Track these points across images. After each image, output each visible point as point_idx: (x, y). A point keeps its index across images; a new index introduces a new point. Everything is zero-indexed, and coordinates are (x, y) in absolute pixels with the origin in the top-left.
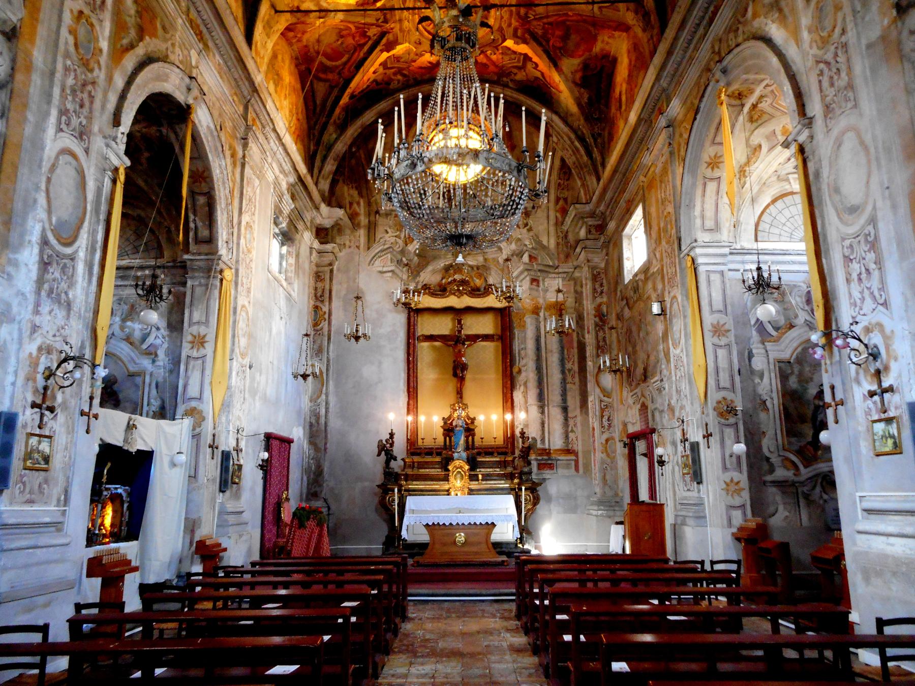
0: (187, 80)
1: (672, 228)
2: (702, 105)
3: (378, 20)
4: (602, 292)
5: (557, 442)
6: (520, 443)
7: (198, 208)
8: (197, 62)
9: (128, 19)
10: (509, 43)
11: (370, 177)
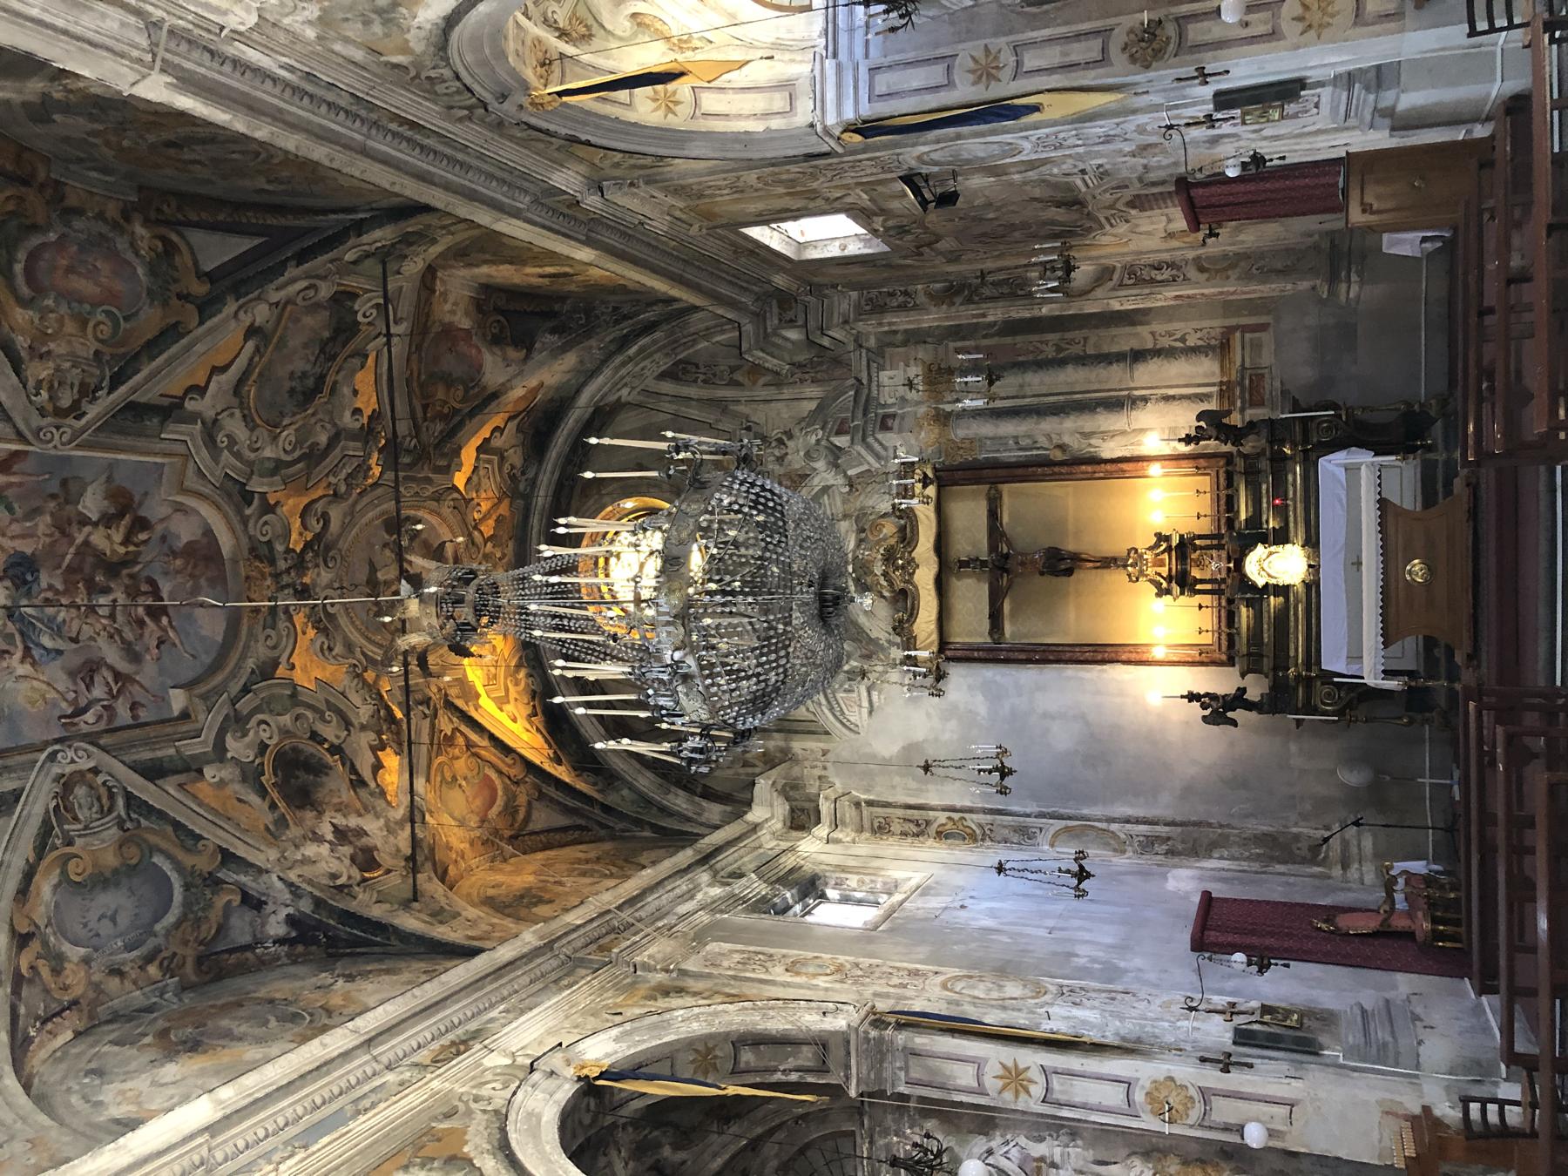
0: (536, 1076)
1: (788, 171)
2: (563, 131)
3: (426, 716)
4: (906, 293)
5: (1205, 371)
6: (1211, 445)
7: (762, 1064)
8: (505, 1053)
10: (460, 480)
11: (704, 770)
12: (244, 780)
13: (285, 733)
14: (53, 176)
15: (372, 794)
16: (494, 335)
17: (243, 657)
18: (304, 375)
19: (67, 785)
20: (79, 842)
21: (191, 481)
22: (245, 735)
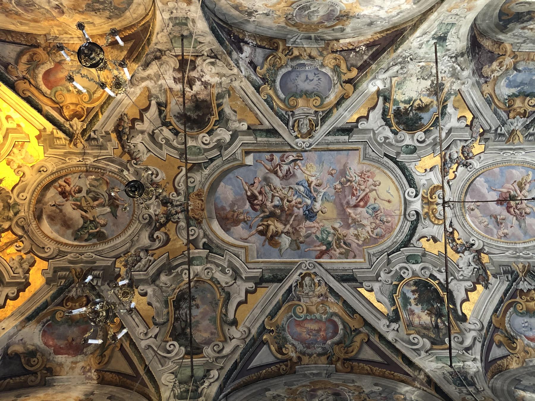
14: (334, 366)
17: (210, 175)
19: (309, 134)
20: (312, 111)
21: (242, 252)
22: (219, 140)
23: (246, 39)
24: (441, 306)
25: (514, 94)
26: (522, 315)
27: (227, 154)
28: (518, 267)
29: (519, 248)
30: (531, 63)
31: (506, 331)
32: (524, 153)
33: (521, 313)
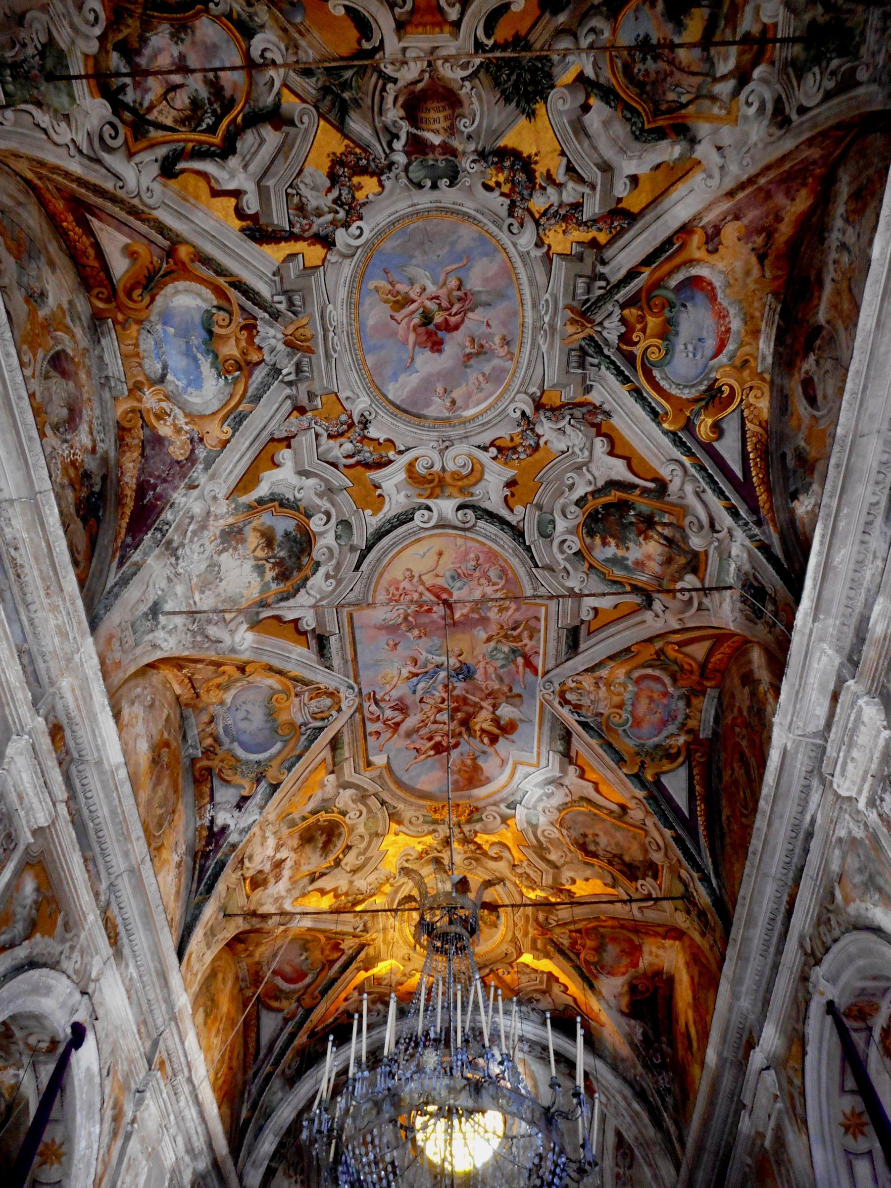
3: (355, 929)
9: (19, 909)
10: (527, 958)
12: (324, 800)
13: (352, 829)
15: (304, 887)
16: (637, 986)
17: (405, 801)
18: (597, 844)
20: (296, 700)
22: (353, 801)
23: (207, 824)
24: (634, 509)
25: (213, 365)
26: (669, 352)
27: (371, 787)
28: (577, 335)
29: (534, 321)
30: (142, 347)
31: (697, 400)
32: (330, 307)
33: (666, 354)
